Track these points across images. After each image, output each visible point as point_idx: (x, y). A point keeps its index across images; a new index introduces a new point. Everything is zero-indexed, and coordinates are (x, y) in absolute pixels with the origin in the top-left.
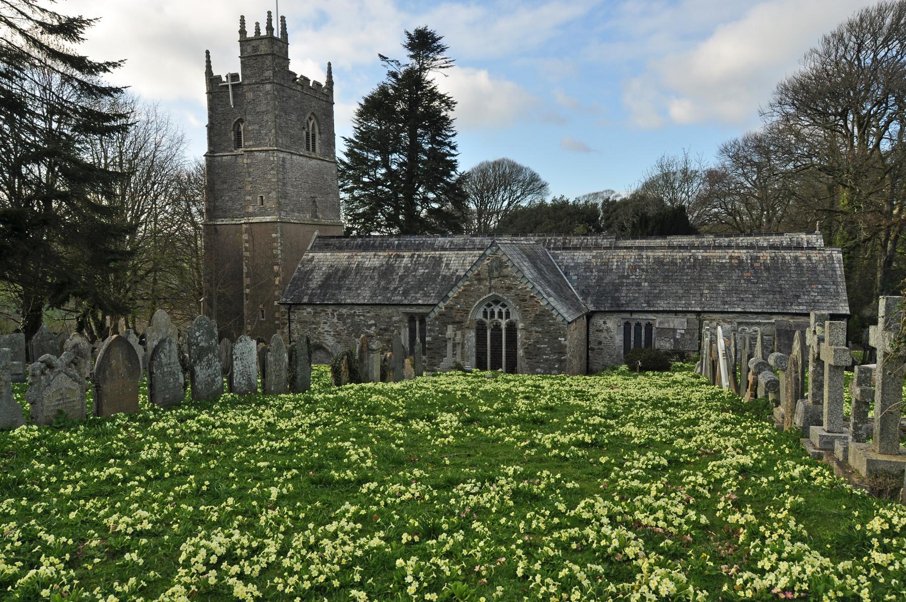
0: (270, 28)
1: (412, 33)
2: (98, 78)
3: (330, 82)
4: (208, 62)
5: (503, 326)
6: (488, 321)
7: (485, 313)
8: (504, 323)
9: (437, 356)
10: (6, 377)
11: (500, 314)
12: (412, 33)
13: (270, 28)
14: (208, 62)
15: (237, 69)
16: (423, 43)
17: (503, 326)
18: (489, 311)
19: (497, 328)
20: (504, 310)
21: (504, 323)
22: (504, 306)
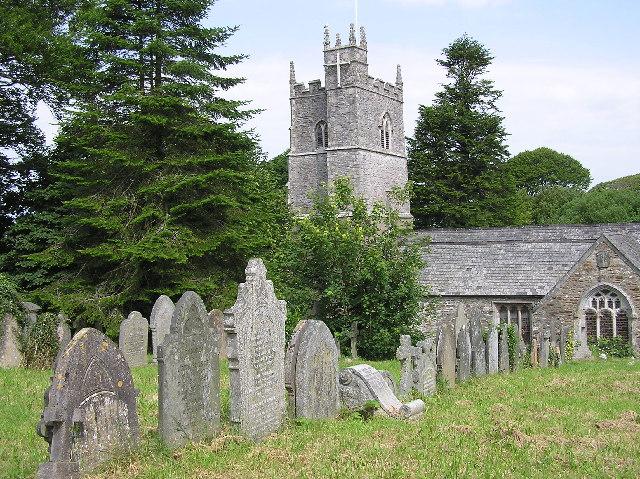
0: (352, 38)
1: (445, 59)
2: (215, 88)
3: (400, 83)
4: (292, 71)
5: (614, 316)
6: (598, 311)
7: (594, 302)
8: (614, 312)
9: (70, 260)
10: (255, 474)
11: (610, 303)
12: (445, 59)
13: (352, 38)
14: (292, 71)
15: (320, 75)
16: (466, 57)
17: (614, 316)
18: (598, 299)
19: (607, 315)
20: (614, 300)
21: (614, 312)
22: (613, 295)
